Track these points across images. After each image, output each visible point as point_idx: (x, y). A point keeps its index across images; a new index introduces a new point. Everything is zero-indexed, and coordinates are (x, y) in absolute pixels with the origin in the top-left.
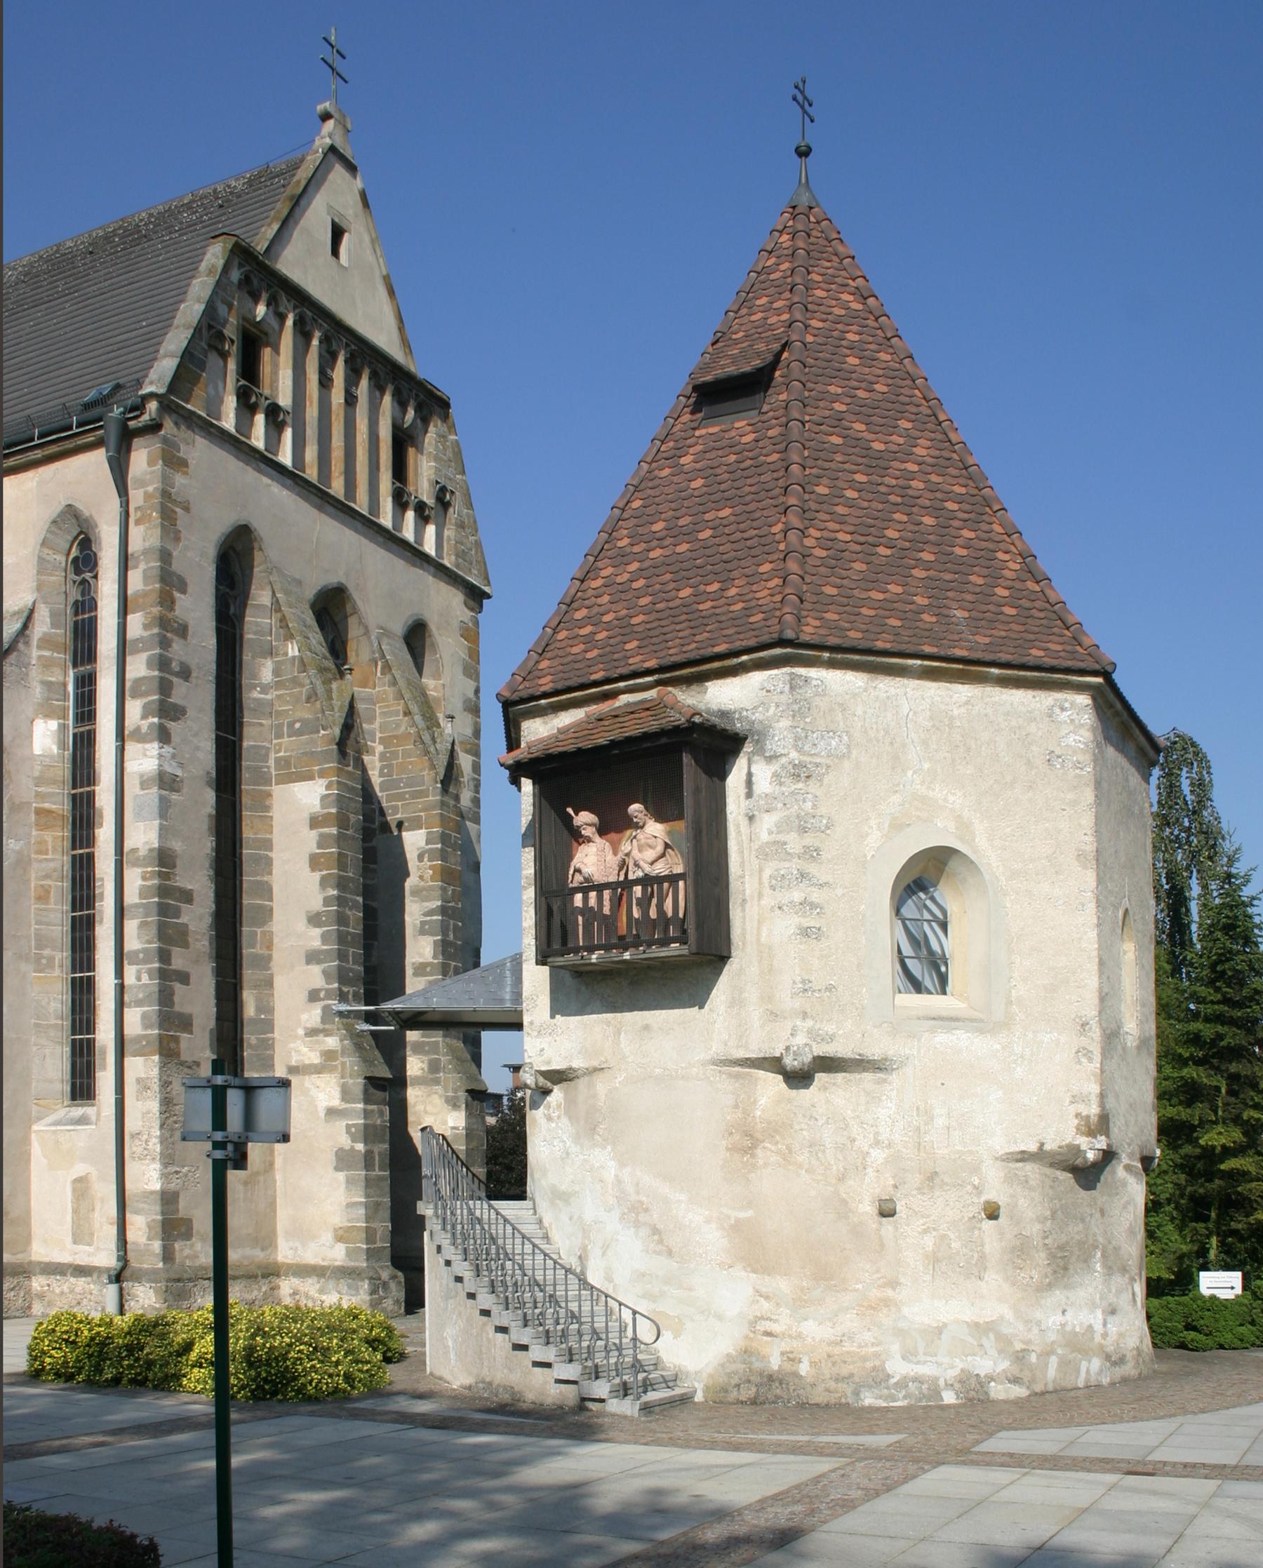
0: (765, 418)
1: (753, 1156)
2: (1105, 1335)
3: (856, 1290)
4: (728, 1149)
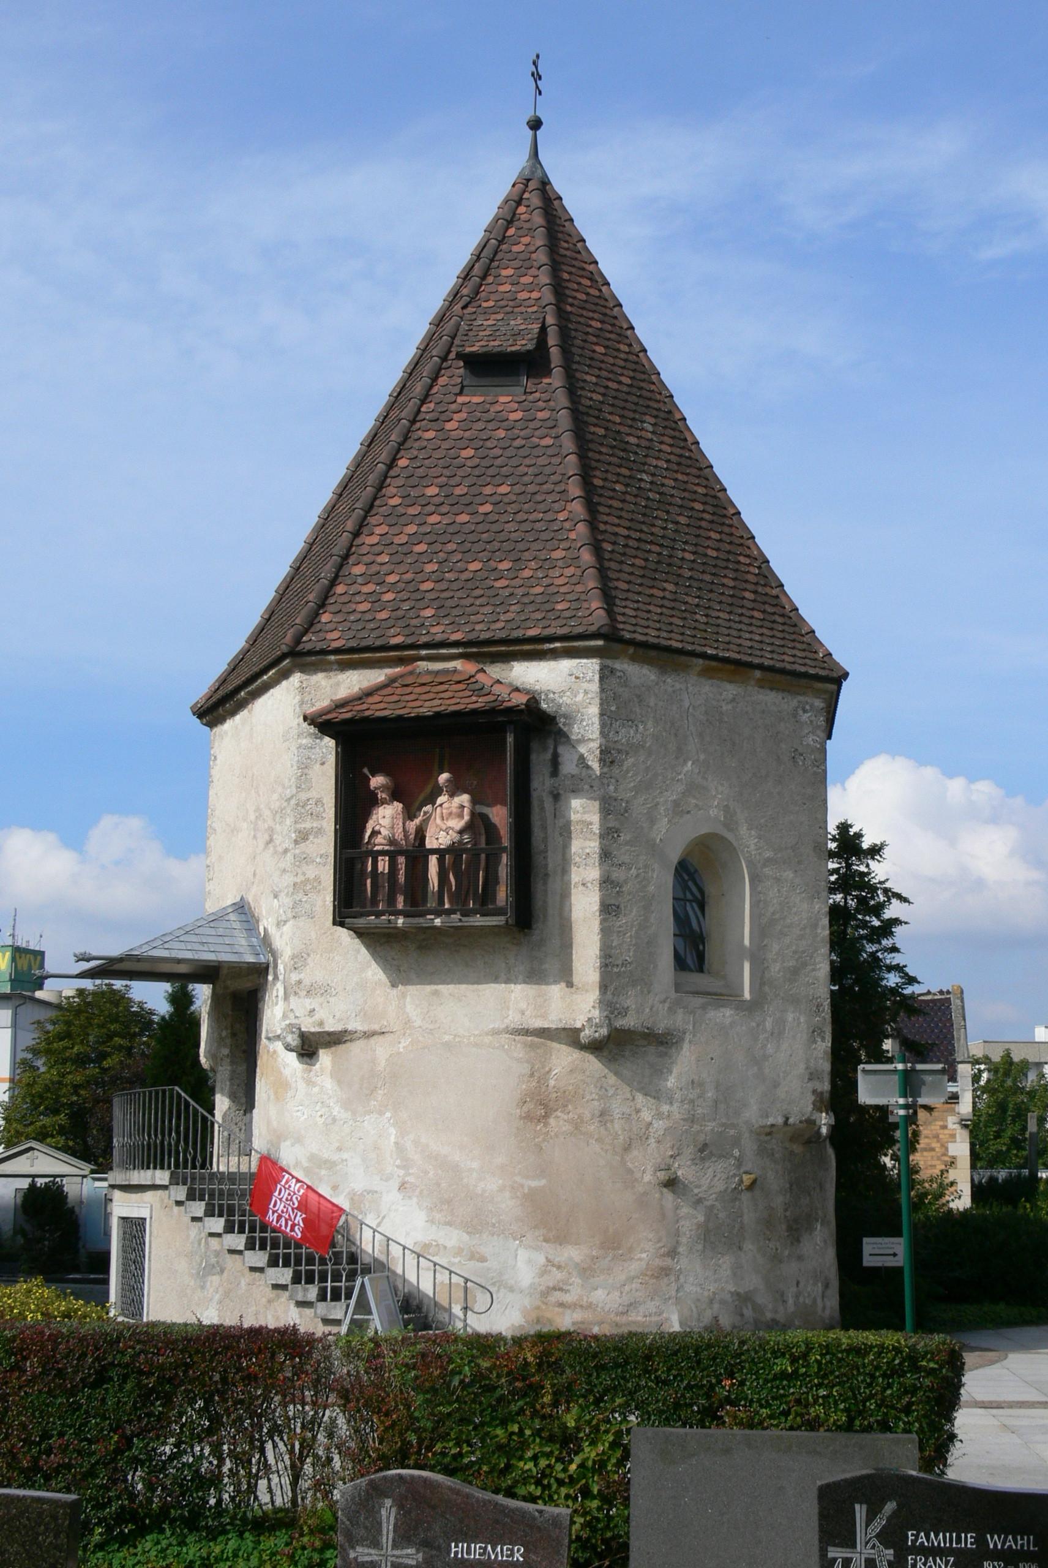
0: (531, 398)
1: (546, 1125)
2: (824, 1308)
3: (640, 1259)
4: (521, 1118)
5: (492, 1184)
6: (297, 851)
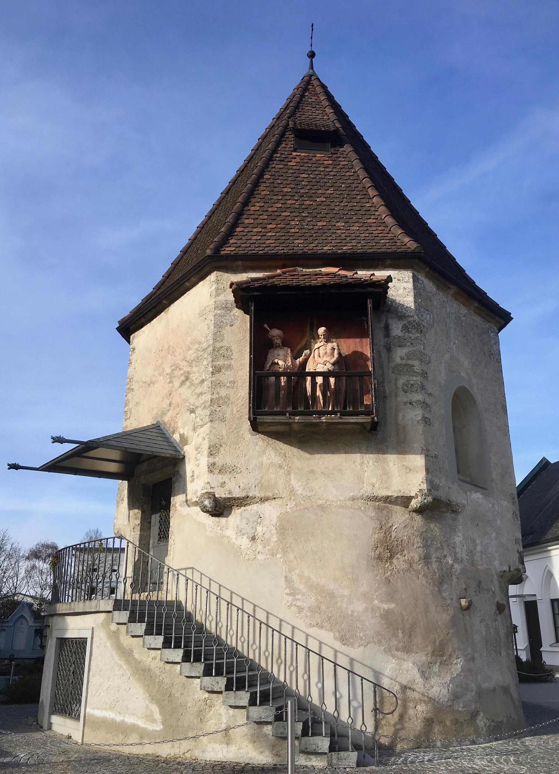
1: (391, 563)
5: (359, 607)
6: (214, 379)
